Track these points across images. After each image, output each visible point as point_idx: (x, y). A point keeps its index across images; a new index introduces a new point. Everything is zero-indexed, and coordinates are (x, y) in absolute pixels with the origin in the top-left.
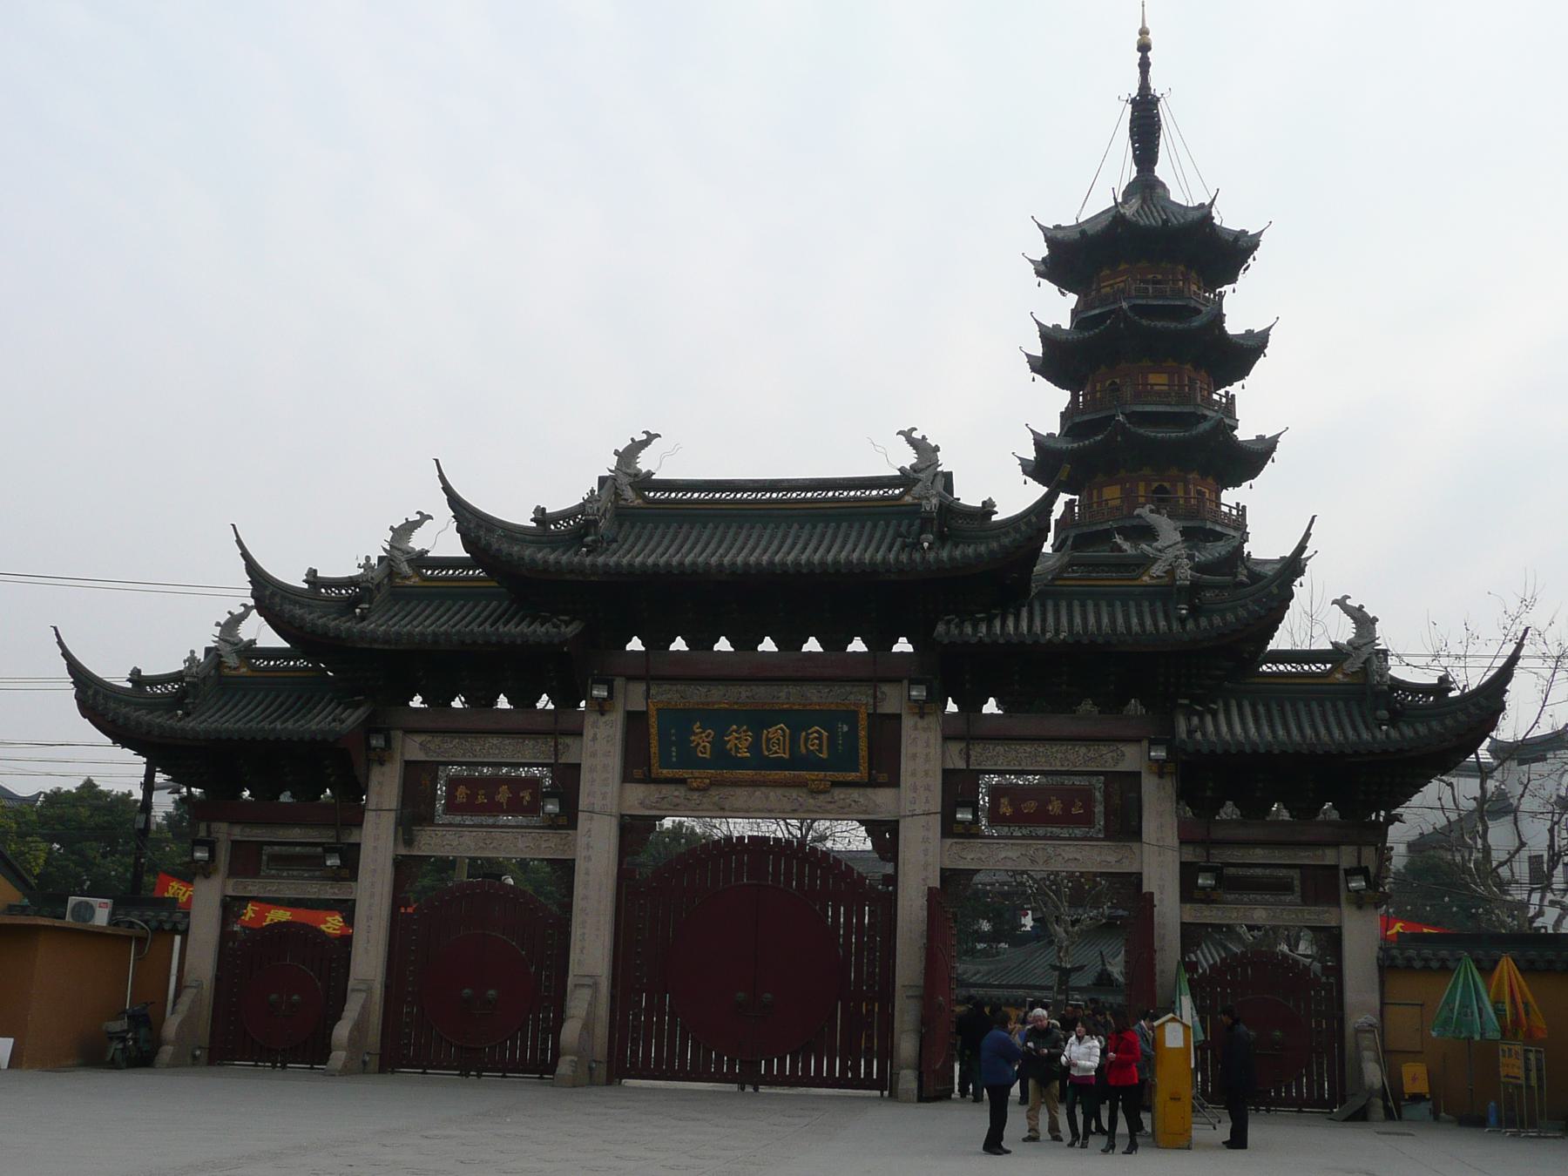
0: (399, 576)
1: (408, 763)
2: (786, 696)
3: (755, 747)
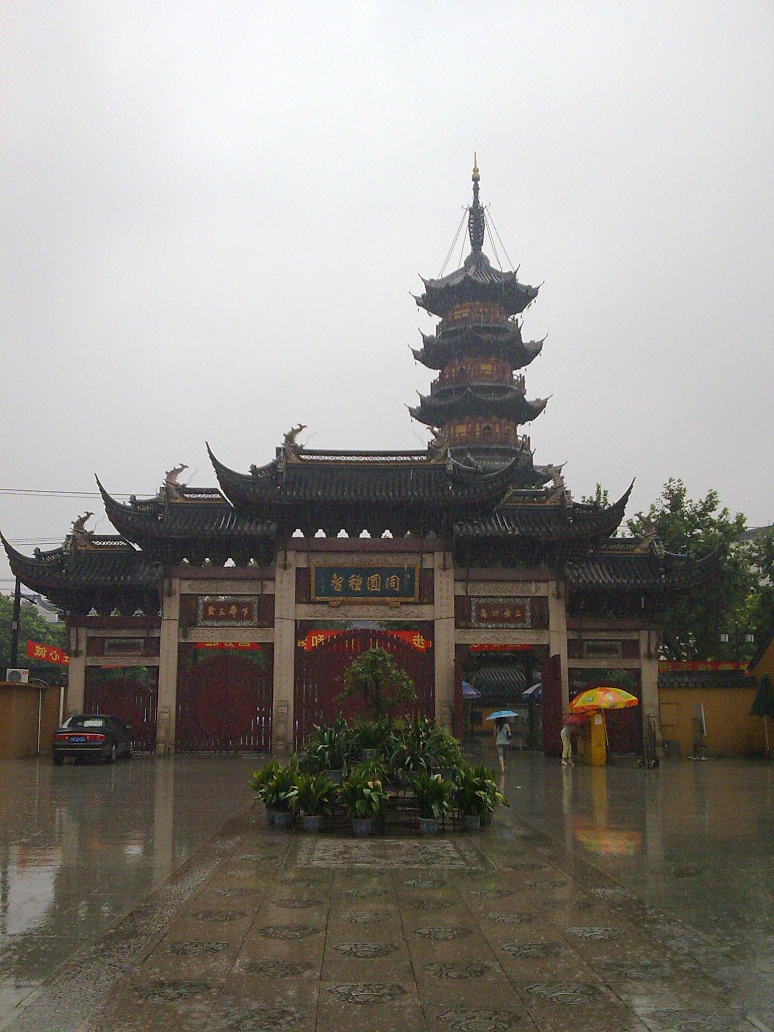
0: (175, 499)
1: (182, 595)
2: (376, 560)
3: (364, 586)
